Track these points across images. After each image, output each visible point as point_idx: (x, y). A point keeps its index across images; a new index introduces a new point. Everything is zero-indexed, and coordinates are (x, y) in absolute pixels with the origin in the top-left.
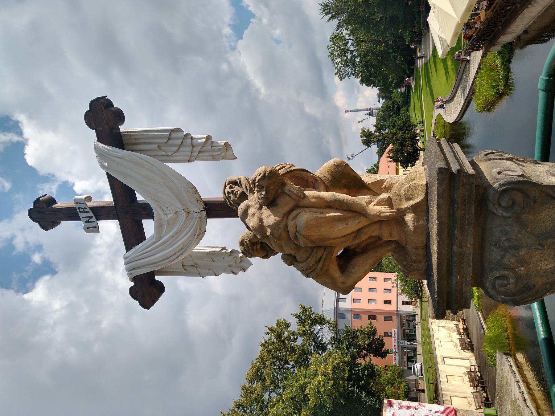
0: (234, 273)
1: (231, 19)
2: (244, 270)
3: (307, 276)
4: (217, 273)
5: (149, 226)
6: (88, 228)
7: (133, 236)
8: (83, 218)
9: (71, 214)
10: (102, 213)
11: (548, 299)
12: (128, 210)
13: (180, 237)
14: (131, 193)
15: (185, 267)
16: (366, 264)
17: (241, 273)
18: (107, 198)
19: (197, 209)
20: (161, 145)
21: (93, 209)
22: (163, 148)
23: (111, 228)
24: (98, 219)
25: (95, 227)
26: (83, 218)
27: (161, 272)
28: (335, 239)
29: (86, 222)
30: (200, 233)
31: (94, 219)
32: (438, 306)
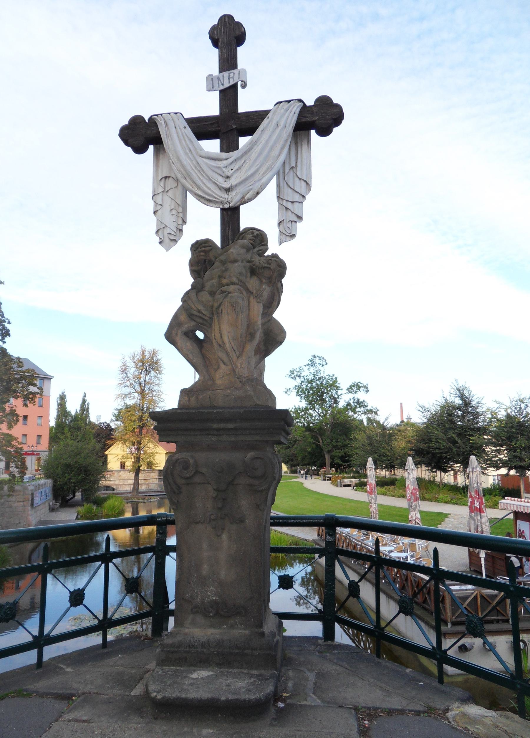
0: (157, 232)
1: (62, 575)
2: (160, 243)
3: (220, 20)
4: (158, 213)
5: (212, 146)
6: (212, 79)
7: (202, 128)
8: (223, 76)
9: (228, 62)
10: (229, 96)
11: (105, 341)
12: (230, 125)
13: (202, 178)
14: (250, 131)
15: (164, 179)
16: (193, 356)
17: (157, 239)
18: (246, 103)
19: (233, 199)
20: (294, 170)
21: (234, 87)
22: (291, 172)
23: (210, 106)
24: (221, 92)
25: (213, 87)
26: (223, 76)
27: (157, 153)
28: (220, 327)
29: (218, 78)
30: (207, 201)
31: (222, 88)
32: (19, 541)
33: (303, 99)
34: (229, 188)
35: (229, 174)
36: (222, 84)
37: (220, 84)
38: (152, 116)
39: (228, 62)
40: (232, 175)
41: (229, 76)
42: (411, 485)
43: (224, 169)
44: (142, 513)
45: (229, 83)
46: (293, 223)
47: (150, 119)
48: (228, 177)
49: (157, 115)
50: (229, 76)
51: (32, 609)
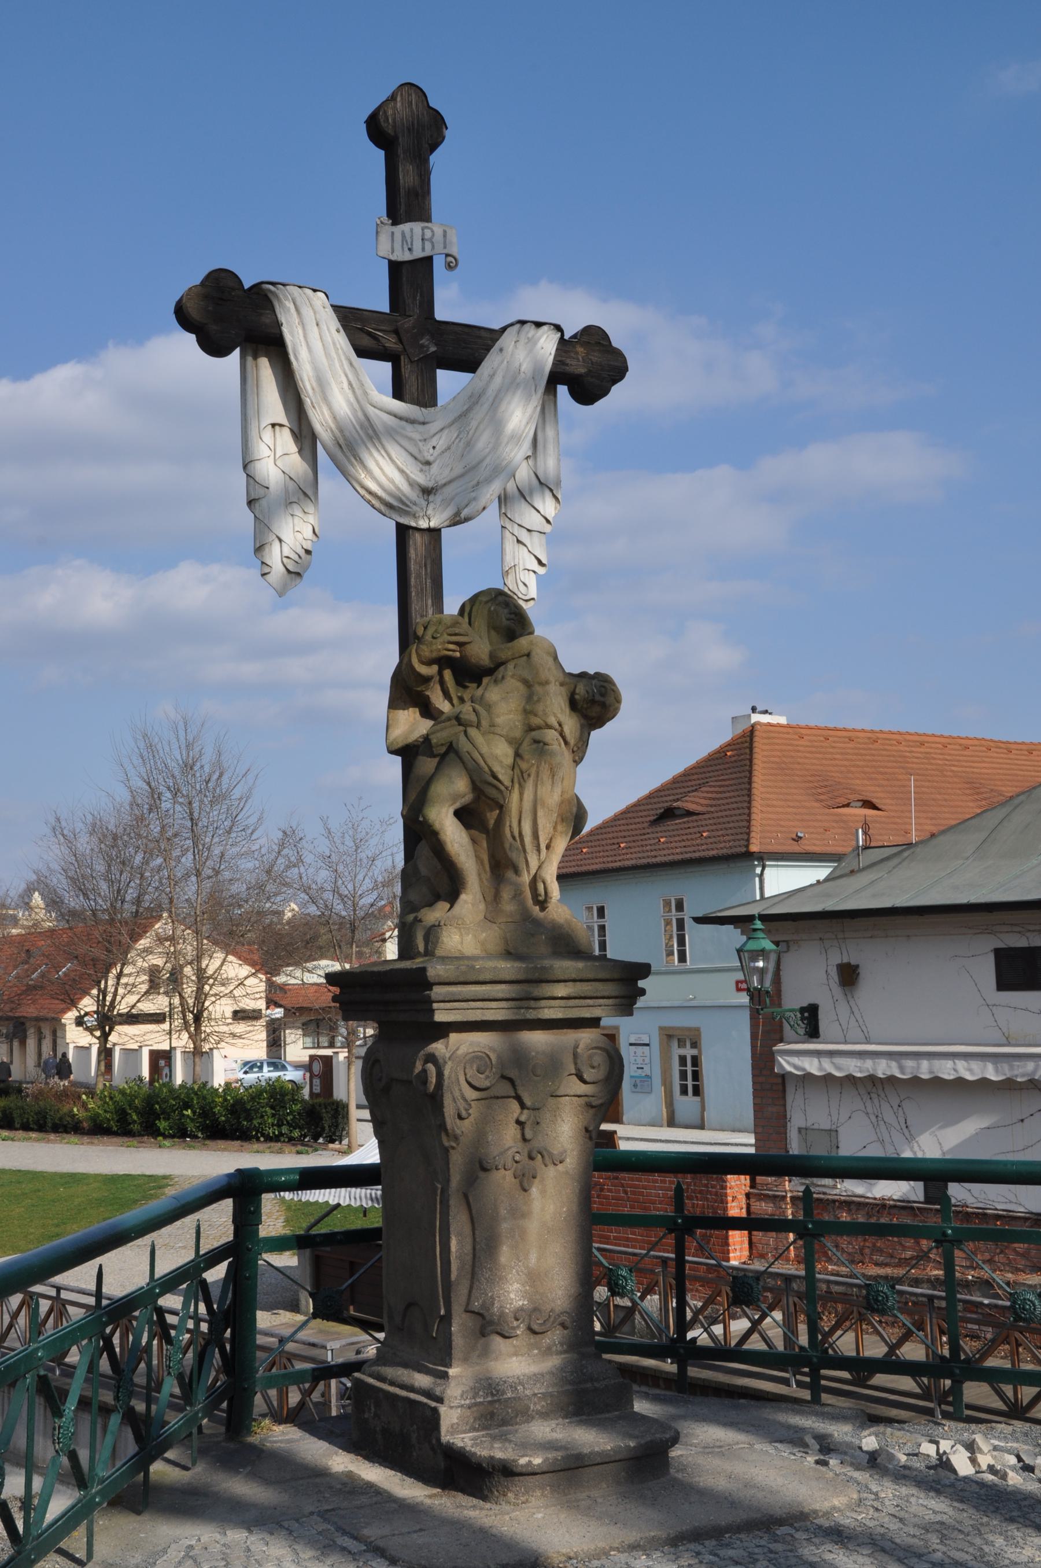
8: (412, 230)
9: (406, 202)
33: (563, 326)
34: (433, 488)
35: (431, 459)
36: (410, 249)
37: (406, 249)
38: (262, 283)
39: (406, 202)
40: (434, 461)
41: (423, 234)
42: (695, 1052)
43: (421, 444)
44: (189, 835)
45: (423, 249)
46: (277, 428)
47: (257, 286)
48: (428, 463)
49: (273, 284)
50: (423, 234)
51: (64, 1306)
